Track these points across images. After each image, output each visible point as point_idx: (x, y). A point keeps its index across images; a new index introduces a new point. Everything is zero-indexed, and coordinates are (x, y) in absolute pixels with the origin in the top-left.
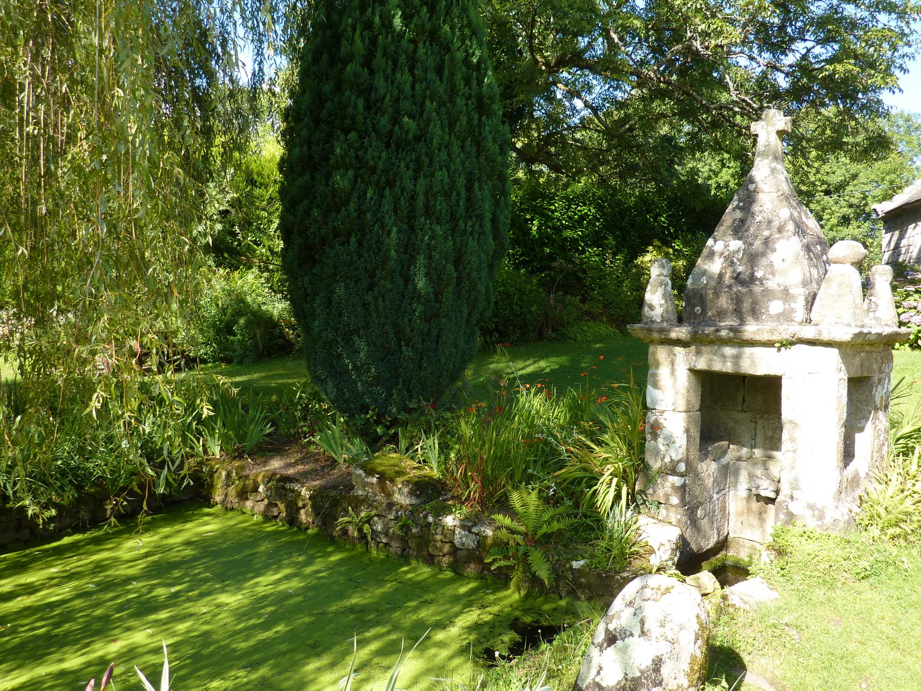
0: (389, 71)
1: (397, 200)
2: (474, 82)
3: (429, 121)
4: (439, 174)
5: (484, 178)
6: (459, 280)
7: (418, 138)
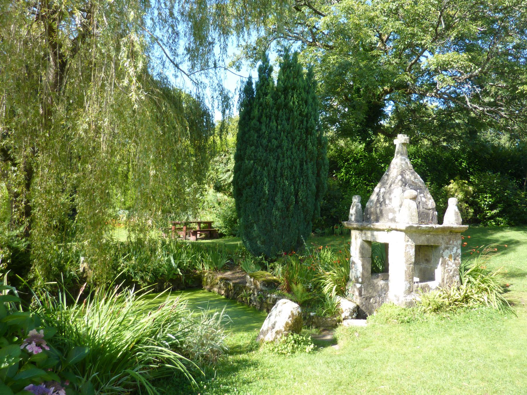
0: (268, 122)
1: (269, 172)
2: (305, 122)
3: (282, 140)
4: (286, 161)
5: (309, 160)
6: (297, 202)
7: (278, 147)
